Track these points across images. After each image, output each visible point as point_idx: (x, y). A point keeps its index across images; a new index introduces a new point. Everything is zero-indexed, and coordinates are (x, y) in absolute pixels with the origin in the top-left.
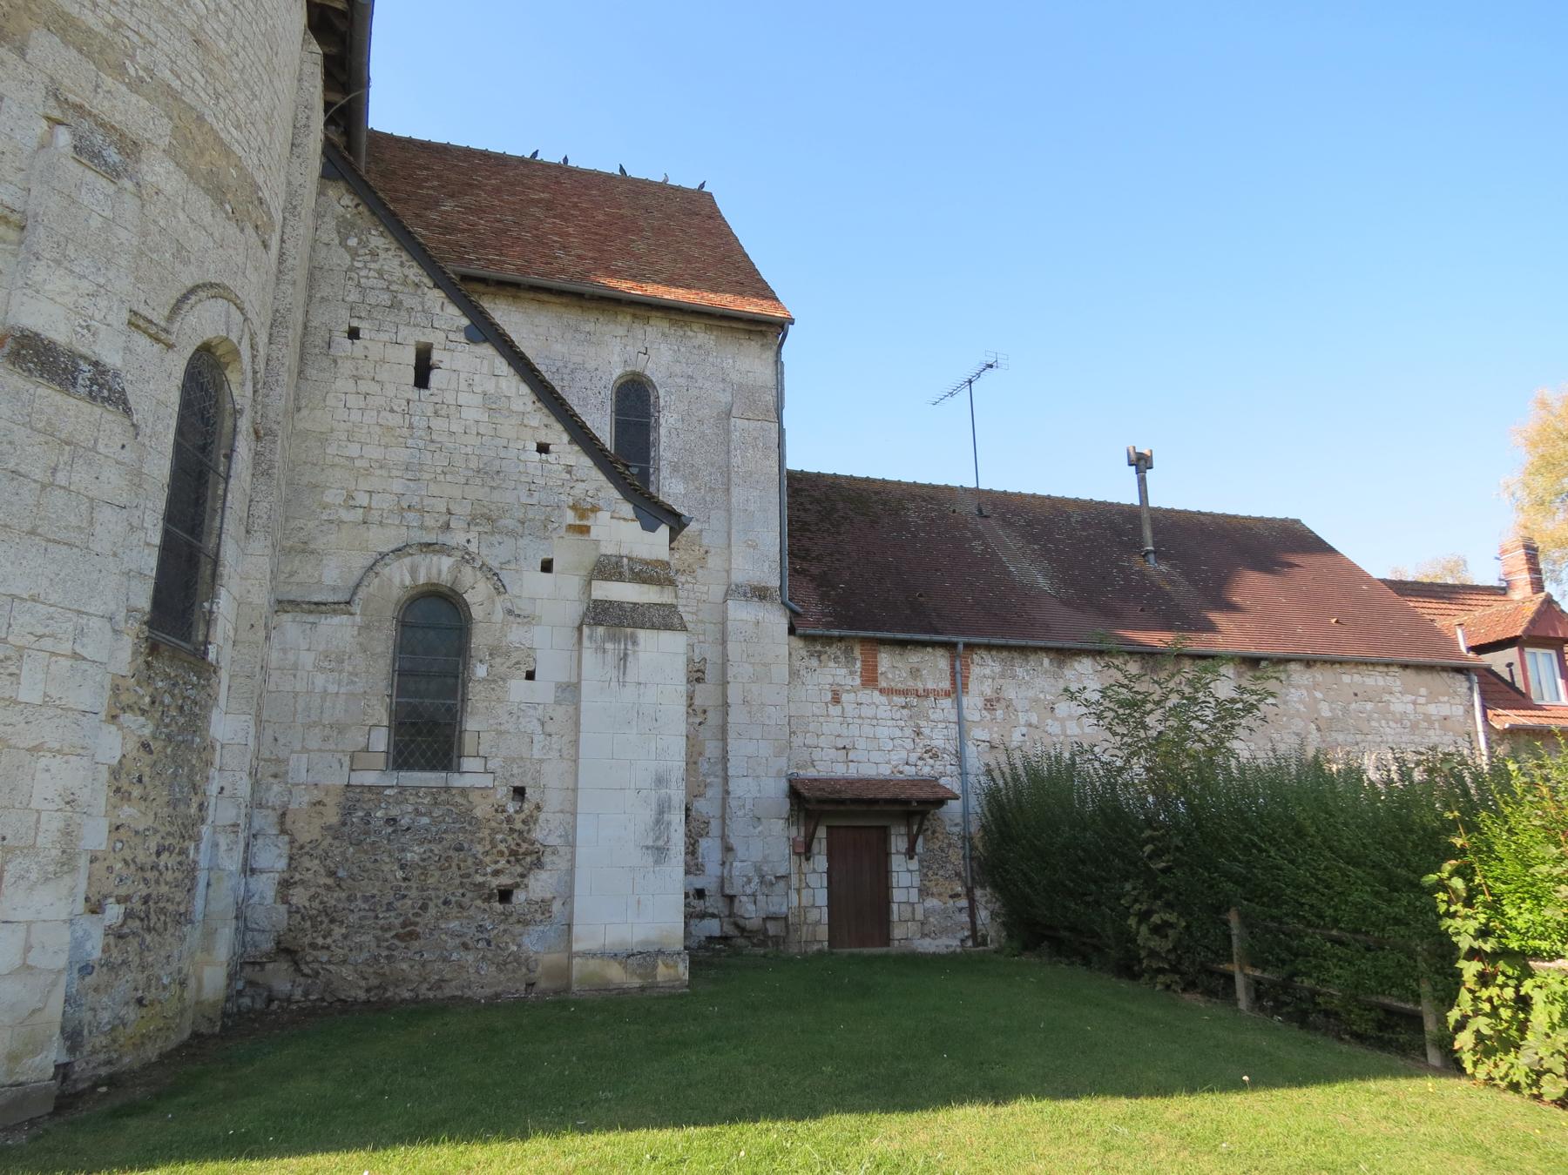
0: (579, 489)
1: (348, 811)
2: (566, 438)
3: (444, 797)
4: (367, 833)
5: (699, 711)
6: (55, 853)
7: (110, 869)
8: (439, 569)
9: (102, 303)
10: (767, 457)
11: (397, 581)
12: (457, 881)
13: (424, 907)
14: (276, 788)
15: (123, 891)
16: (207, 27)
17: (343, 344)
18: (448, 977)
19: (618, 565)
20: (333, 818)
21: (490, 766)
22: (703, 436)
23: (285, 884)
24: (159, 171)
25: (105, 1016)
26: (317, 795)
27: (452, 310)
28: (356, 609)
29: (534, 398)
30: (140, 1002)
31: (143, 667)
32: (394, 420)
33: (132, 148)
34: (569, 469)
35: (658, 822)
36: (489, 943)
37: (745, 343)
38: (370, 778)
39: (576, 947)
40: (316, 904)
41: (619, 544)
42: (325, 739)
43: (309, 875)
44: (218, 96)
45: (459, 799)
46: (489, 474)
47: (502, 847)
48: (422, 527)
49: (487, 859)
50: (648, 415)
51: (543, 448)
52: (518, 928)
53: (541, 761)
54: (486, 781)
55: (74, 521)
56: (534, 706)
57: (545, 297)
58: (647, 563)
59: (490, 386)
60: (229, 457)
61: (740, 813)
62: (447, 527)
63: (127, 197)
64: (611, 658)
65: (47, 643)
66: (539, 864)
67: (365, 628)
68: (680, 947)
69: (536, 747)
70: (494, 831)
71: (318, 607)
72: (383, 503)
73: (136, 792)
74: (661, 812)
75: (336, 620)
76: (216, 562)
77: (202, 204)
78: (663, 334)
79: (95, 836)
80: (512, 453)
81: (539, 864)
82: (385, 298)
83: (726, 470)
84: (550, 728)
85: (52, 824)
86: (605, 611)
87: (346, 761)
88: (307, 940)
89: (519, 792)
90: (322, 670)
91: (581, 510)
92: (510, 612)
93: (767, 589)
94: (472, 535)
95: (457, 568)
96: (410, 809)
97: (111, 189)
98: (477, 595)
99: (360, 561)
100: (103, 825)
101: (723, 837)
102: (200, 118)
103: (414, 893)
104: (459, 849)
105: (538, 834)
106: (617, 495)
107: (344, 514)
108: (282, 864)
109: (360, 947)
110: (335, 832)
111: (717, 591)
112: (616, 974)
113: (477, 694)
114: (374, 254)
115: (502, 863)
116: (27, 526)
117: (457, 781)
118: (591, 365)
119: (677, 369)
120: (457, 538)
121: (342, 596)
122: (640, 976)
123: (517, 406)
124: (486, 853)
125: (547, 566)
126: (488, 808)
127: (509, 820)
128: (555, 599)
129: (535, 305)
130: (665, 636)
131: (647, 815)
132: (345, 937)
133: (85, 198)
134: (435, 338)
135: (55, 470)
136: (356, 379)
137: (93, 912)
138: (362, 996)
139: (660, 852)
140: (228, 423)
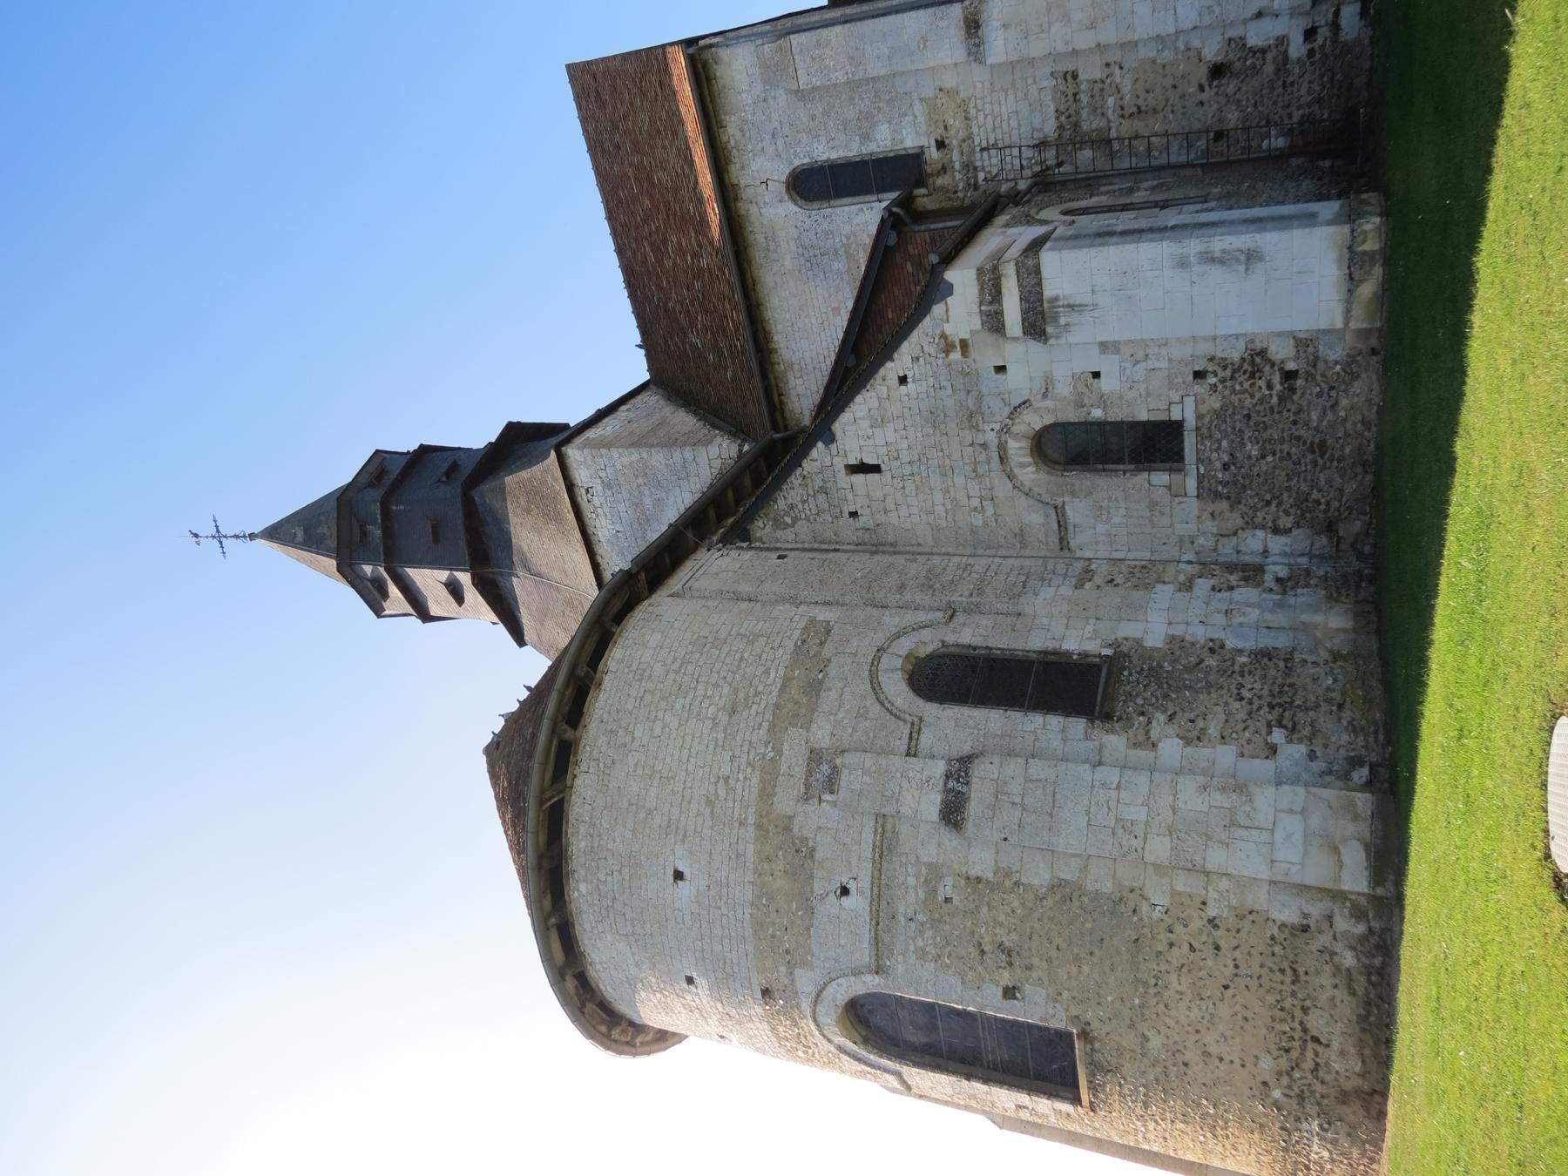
0: (931, 349)
1: (1218, 496)
2: (889, 364)
3: (1204, 431)
4: (1235, 483)
5: (1107, 71)
6: (1234, 797)
7: (1249, 741)
8: (1018, 449)
9: (911, 774)
10: (828, 42)
11: (1033, 476)
12: (1277, 416)
13: (1298, 438)
14: (1202, 541)
15: (1264, 730)
16: (721, 703)
17: (861, 521)
18: (1359, 418)
19: (988, 314)
20: (1224, 505)
21: (1177, 399)
22: (826, 113)
23: (1276, 531)
24: (821, 733)
25: (1345, 738)
26: (1206, 516)
27: (814, 453)
28: (1059, 501)
29: (864, 391)
30: (1340, 707)
31: (1121, 724)
32: (910, 486)
33: (815, 756)
34: (916, 359)
35: (1222, 262)
36: (1332, 388)
37: (721, 83)
38: (1191, 484)
39: (1339, 325)
40: (1292, 511)
41: (970, 314)
42: (1162, 514)
43: (1269, 518)
44: (757, 694)
45: (1206, 420)
46: (934, 419)
47: (1246, 385)
48: (988, 462)
49: (1258, 395)
50: (822, 168)
51: (903, 380)
52: (1321, 366)
53: (1170, 360)
54: (1190, 403)
55: (1040, 792)
56: (1122, 370)
57: (749, 282)
58: (982, 289)
59: (865, 424)
60: (975, 648)
61: (1217, 10)
62: (984, 446)
63: (846, 761)
64: (1074, 318)
65: (1113, 805)
66: (1263, 353)
67: (1073, 493)
68: (1346, 229)
69: (1157, 365)
70: (1234, 391)
71: (1062, 525)
72: (974, 488)
73: (1200, 723)
74: (1213, 260)
75: (1070, 513)
76: (1046, 653)
77: (828, 698)
78: (743, 168)
79: (1225, 755)
80: (914, 404)
81: (1263, 353)
82: (821, 498)
83: (853, 85)
84: (1140, 356)
85: (1217, 798)
86: (1032, 326)
87: (1177, 500)
88: (1321, 516)
89: (1199, 375)
90: (1109, 519)
91: (948, 348)
92: (1045, 396)
93: (966, 19)
94: (987, 427)
95: (1016, 437)
96: (1215, 454)
97: (845, 772)
98: (1034, 421)
99: (1023, 501)
100: (1221, 749)
101: (1245, 22)
102: (777, 706)
103: (1286, 447)
104: (1248, 417)
105: (1236, 356)
106: (927, 319)
107: (990, 511)
108: (1260, 534)
109: (1329, 481)
110: (1235, 503)
111: (979, 73)
112: (1367, 290)
113: (1116, 415)
114: (792, 507)
115: (1261, 383)
116: (1048, 819)
117: (1190, 422)
118: (794, 232)
119: (770, 150)
120: (991, 438)
121: (1052, 512)
122: (1372, 266)
123: (874, 403)
124: (1252, 396)
125: (1001, 369)
126: (1214, 397)
127: (1223, 381)
128: (1026, 365)
129: (758, 287)
130: (1046, 272)
131: (1216, 272)
132: (1320, 490)
133: (856, 786)
134: (840, 464)
135: (1014, 803)
136: (886, 512)
137: (1275, 752)
138: (1369, 477)
139: (1251, 257)
140: (952, 650)
